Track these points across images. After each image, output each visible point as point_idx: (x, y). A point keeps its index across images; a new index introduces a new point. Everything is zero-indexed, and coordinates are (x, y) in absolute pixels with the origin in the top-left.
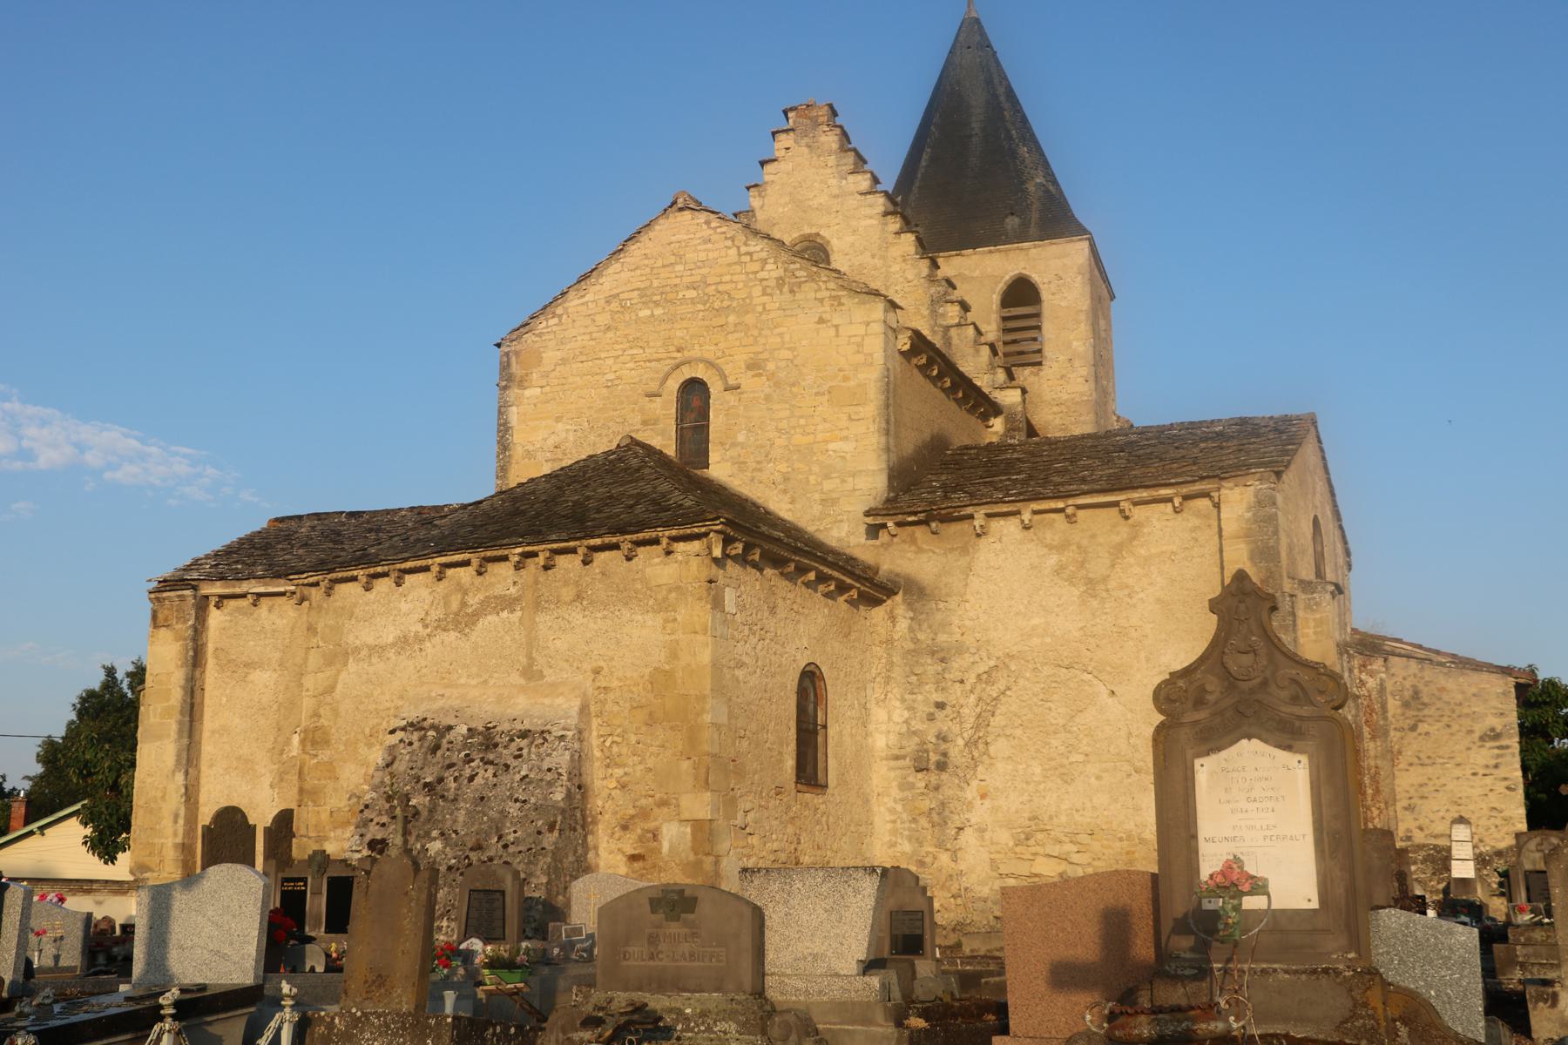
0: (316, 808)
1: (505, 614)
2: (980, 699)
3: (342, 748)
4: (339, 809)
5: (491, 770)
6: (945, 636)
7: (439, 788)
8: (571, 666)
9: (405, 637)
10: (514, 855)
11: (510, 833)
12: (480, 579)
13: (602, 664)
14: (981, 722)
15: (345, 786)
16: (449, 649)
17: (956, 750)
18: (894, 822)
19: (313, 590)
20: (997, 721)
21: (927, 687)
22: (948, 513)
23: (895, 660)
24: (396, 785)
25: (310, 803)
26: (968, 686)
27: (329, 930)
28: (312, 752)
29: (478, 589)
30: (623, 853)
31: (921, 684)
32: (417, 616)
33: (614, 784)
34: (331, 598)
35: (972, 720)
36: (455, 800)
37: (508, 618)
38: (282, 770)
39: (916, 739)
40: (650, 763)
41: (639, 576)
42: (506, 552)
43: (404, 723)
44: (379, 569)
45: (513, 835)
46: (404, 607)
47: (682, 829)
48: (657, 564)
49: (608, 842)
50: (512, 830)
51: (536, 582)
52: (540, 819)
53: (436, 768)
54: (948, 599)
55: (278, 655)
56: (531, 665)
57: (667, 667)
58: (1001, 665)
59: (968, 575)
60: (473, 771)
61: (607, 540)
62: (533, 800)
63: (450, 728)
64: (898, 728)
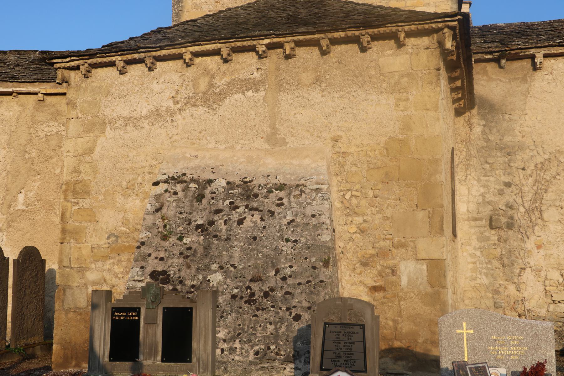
0: (78, 245)
1: (250, 93)
2: (536, 181)
3: (101, 197)
4: (99, 246)
5: (257, 216)
6: (510, 137)
7: (211, 229)
8: (312, 135)
9: (157, 111)
10: (294, 286)
11: (286, 268)
12: (226, 66)
13: (340, 133)
14: (537, 197)
15: (105, 227)
16: (198, 120)
17: (519, 215)
18: (475, 263)
19: (73, 73)
20: (549, 196)
21: (497, 172)
22: (516, 53)
23: (472, 153)
24: (168, 227)
25: (72, 240)
26: (528, 172)
27: (166, 358)
28: (73, 200)
29: (224, 74)
30: (365, 285)
31: (492, 169)
32: (168, 94)
33: (355, 229)
34: (89, 79)
35: (531, 195)
36: (228, 239)
37: (253, 96)
38: (9, 219)
39: (490, 207)
40: (388, 212)
41: (373, 64)
42: (255, 43)
43: (165, 177)
44: (136, 56)
45: (289, 269)
46: (156, 87)
47: (418, 266)
48: (389, 55)
49: (350, 276)
50: (288, 265)
51: (278, 69)
52: (313, 256)
53: (204, 213)
54: (512, 113)
55: (6, 137)
56: (274, 134)
57: (401, 137)
58: (553, 158)
59: (527, 97)
60: (240, 215)
61: (350, 33)
62: (303, 240)
63: (210, 182)
64: (476, 200)
